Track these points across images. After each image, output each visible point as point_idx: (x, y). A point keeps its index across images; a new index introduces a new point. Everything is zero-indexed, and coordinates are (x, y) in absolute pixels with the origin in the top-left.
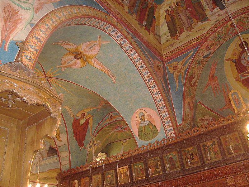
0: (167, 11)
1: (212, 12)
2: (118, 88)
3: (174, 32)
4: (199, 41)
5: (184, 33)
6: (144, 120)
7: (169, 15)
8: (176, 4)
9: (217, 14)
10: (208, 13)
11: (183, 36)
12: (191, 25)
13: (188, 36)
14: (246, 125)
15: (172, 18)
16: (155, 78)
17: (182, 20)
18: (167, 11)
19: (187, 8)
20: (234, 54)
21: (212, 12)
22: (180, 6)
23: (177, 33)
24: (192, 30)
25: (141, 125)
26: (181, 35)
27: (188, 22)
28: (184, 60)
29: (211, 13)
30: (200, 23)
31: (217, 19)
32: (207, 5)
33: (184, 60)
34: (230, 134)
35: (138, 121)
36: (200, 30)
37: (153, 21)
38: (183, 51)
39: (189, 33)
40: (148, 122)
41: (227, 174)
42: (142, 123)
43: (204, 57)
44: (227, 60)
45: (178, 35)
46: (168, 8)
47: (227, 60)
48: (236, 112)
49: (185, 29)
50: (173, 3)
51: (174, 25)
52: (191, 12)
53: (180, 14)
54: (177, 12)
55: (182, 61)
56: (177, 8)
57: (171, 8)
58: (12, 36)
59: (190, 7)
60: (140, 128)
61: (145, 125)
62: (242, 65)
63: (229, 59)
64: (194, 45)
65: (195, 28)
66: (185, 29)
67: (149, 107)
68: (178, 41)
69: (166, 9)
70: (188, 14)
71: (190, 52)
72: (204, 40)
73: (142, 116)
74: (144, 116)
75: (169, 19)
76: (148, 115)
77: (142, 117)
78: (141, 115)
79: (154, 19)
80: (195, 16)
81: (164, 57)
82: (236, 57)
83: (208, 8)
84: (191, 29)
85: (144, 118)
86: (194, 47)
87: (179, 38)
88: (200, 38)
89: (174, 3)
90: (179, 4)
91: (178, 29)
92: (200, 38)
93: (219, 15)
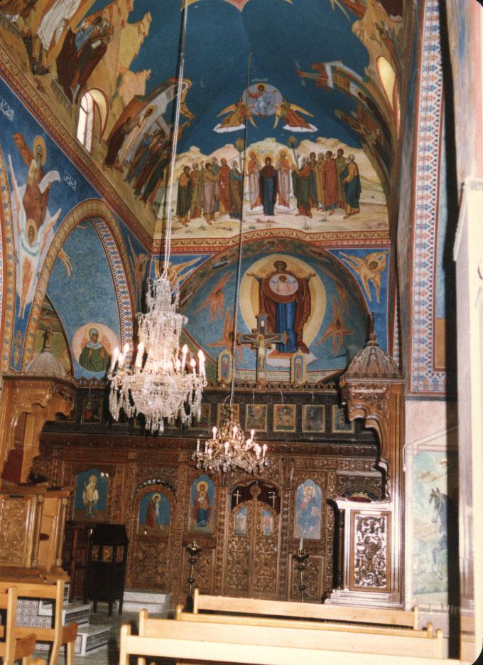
0: (186, 168)
1: (252, 208)
2: (72, 283)
3: (185, 208)
4: (215, 245)
5: (198, 219)
6: (96, 341)
7: (188, 176)
8: (204, 165)
9: (257, 217)
10: (246, 207)
11: (196, 223)
12: (214, 212)
13: (203, 228)
14: (385, 196)
15: (190, 184)
16: (132, 291)
17: (204, 194)
18: (186, 168)
19: (220, 181)
20: (262, 270)
21: (252, 208)
22: (210, 171)
23: (189, 213)
24: (212, 222)
25: (87, 346)
26: (193, 220)
27: (211, 205)
28: (183, 266)
29: (249, 210)
30: (228, 216)
31: (253, 225)
32: (250, 192)
33: (183, 266)
34: (258, 158)
35: (85, 339)
36: (224, 228)
37: (159, 181)
38: (185, 250)
39: (205, 224)
40: (100, 346)
41: (182, 447)
42: (91, 343)
43: (214, 268)
44: (248, 275)
45: (189, 217)
46: (190, 165)
47: (248, 275)
48: (219, 379)
49: (202, 213)
50: (200, 161)
51: (189, 197)
52: (222, 190)
53: (206, 184)
54: (202, 180)
55: (179, 265)
56: (205, 172)
57: (194, 168)
58: (38, 259)
59: (224, 182)
60: (86, 350)
61: (95, 348)
62: (270, 289)
63: (252, 275)
64: (206, 249)
65: (219, 221)
66: (202, 213)
67: (110, 327)
68: (185, 229)
69: (185, 165)
70: (217, 192)
71: (196, 257)
72: (222, 249)
73: (94, 334)
74: (97, 335)
75: (185, 184)
76: (105, 337)
77: (95, 336)
78: (94, 332)
79: (160, 178)
80: (226, 201)
81: (154, 244)
82: (263, 276)
83: (248, 199)
84: (211, 219)
85: (97, 339)
86: (205, 252)
87: (188, 224)
88: (217, 242)
89: (203, 162)
90: (210, 168)
91: (193, 206)
92: (217, 242)
93: (259, 221)
